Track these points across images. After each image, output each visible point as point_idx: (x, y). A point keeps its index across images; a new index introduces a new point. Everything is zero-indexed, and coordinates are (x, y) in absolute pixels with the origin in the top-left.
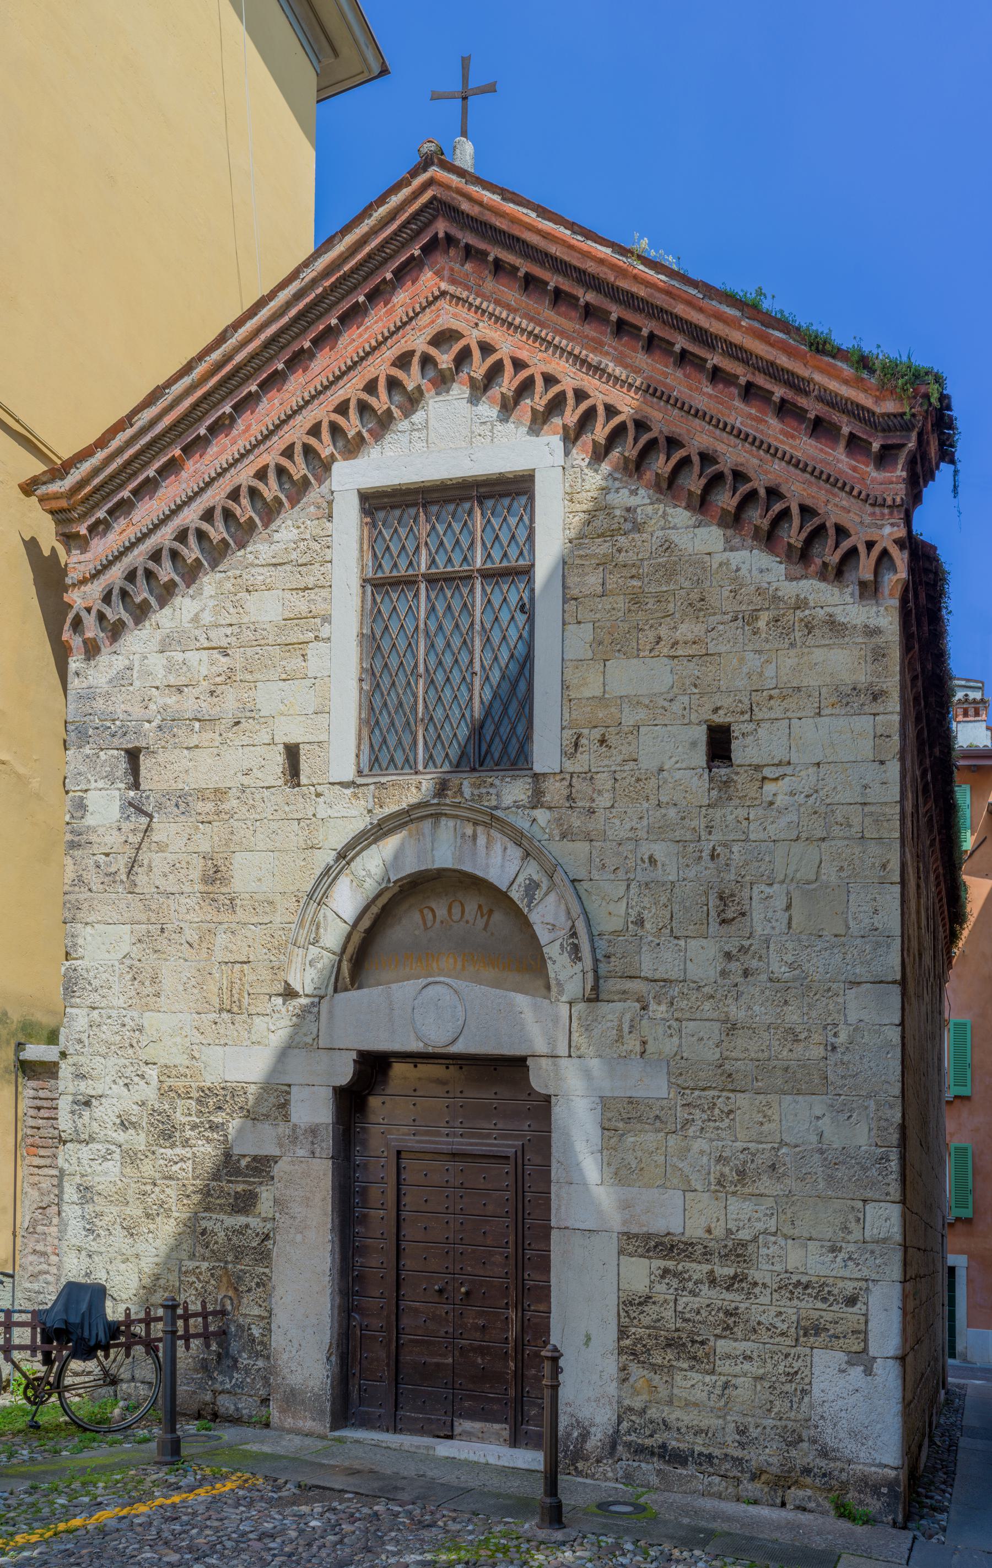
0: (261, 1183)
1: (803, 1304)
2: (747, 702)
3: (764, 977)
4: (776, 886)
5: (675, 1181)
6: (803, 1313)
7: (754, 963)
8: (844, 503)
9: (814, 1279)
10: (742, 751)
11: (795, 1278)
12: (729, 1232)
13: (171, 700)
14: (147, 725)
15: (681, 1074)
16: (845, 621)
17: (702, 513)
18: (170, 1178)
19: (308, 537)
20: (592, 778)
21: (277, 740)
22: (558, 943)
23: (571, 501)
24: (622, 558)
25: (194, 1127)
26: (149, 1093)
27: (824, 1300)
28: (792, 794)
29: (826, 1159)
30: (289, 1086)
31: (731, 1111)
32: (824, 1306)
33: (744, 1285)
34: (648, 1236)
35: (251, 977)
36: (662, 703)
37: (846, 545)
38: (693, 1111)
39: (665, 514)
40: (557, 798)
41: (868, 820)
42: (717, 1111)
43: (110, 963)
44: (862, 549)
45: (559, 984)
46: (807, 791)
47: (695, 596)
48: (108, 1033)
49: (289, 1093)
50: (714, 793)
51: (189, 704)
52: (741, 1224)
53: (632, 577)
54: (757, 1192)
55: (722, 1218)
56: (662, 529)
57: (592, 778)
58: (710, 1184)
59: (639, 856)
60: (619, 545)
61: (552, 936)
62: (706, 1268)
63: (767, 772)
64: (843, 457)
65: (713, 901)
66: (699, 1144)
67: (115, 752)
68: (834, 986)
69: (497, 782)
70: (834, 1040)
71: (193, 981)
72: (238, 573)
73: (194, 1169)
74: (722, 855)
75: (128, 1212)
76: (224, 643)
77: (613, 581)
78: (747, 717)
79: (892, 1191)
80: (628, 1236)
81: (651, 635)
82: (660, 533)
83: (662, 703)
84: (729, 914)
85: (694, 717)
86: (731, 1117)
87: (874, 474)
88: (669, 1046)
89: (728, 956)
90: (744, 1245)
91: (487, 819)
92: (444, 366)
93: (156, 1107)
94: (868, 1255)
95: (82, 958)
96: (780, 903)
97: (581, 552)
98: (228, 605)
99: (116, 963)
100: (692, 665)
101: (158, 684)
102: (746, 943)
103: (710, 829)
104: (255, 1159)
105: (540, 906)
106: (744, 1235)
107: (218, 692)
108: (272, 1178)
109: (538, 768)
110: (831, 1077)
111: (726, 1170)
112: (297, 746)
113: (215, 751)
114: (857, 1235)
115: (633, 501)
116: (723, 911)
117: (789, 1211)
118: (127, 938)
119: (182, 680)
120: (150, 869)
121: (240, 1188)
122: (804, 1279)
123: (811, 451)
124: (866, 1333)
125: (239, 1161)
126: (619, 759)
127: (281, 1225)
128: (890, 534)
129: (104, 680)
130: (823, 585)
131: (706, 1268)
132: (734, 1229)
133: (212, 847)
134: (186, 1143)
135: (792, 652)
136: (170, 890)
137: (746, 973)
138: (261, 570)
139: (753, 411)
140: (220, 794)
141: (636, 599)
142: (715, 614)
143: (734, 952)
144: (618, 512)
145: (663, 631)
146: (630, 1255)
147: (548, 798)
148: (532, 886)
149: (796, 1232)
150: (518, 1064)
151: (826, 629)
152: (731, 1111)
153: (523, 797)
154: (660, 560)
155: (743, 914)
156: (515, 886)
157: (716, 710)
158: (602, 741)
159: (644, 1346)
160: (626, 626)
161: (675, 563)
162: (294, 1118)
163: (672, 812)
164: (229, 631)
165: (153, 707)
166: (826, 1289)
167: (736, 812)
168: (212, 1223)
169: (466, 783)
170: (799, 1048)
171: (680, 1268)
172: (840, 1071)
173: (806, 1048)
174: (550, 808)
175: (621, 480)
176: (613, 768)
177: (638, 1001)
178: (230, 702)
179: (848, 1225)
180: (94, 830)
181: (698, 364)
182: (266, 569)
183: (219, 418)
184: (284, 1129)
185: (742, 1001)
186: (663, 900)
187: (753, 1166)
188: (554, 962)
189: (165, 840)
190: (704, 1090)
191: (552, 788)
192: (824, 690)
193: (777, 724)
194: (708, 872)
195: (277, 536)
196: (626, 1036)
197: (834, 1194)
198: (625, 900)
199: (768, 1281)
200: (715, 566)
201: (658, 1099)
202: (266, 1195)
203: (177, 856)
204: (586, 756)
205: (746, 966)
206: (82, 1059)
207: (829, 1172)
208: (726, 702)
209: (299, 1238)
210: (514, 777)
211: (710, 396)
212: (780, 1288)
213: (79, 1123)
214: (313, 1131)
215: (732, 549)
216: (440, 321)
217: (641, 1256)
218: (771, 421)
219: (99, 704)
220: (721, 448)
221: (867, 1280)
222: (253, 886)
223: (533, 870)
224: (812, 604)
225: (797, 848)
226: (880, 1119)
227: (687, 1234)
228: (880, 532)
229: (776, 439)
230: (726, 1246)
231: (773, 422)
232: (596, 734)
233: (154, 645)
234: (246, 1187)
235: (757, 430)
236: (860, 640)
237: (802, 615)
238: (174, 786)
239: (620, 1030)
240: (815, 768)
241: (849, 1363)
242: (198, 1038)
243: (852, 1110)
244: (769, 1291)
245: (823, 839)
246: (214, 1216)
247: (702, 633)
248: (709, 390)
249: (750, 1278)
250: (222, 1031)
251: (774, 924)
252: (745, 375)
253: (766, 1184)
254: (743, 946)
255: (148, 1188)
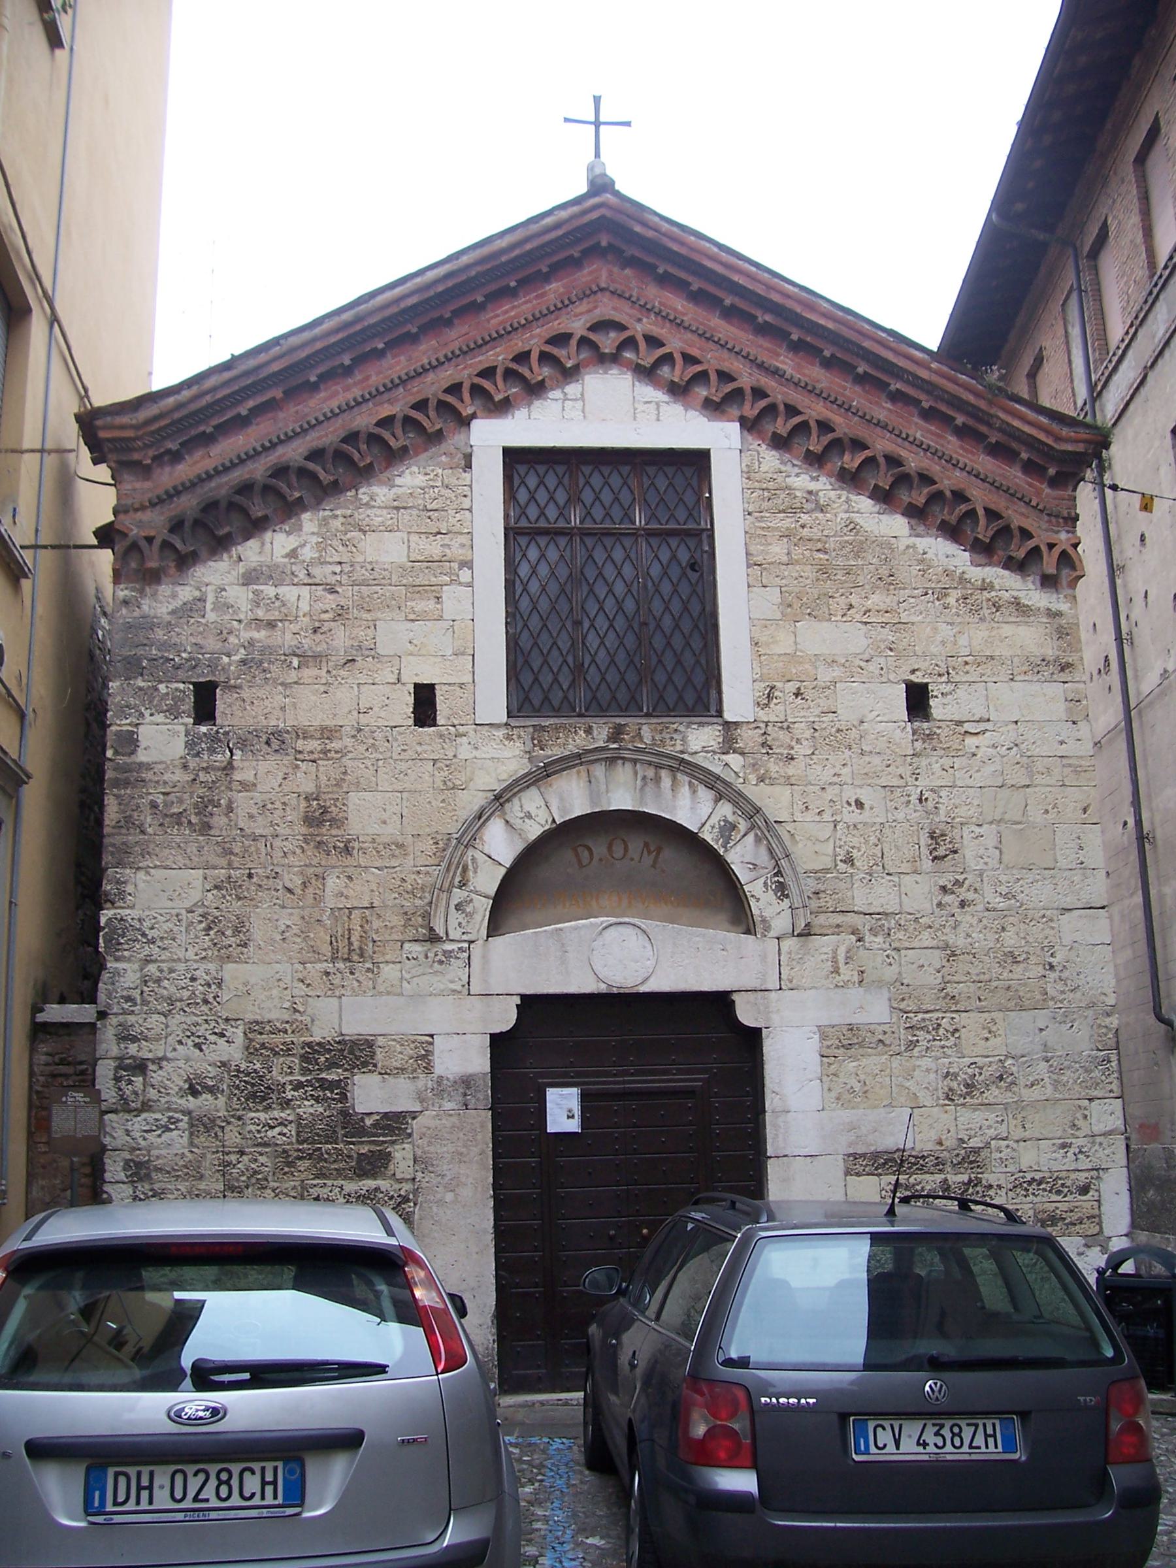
0: (393, 1142)
1: (1038, 1199)
2: (943, 666)
3: (980, 907)
4: (985, 826)
5: (902, 1099)
6: (1040, 1207)
7: (970, 896)
8: (1023, 510)
9: (1047, 1175)
10: (936, 706)
11: (1029, 1177)
12: (962, 1141)
13: (260, 635)
14: (225, 659)
15: (903, 999)
16: (1030, 603)
17: (885, 503)
18: (266, 1145)
19: (439, 484)
20: (788, 727)
21: (404, 679)
22: (762, 880)
23: (748, 478)
24: (805, 532)
25: (298, 1086)
26: (233, 1051)
27: (1059, 1192)
28: (994, 746)
29: (1051, 1066)
30: (432, 1036)
31: (956, 1030)
32: (1059, 1198)
33: (978, 1188)
34: (876, 1155)
35: (376, 924)
36: (858, 662)
37: (1031, 544)
38: (918, 1033)
39: (848, 501)
40: (751, 744)
41: (1067, 770)
42: (941, 1031)
43: (174, 912)
44: (1044, 548)
45: (764, 921)
46: (1008, 744)
47: (884, 572)
48: (173, 989)
49: (432, 1044)
50: (918, 745)
51: (285, 638)
52: (973, 1133)
53: (818, 550)
54: (987, 1101)
55: (953, 1129)
56: (847, 512)
57: (788, 727)
58: (938, 1098)
59: (845, 800)
60: (802, 521)
61: (753, 875)
62: (939, 1178)
63: (967, 727)
64: (1019, 474)
65: (924, 840)
66: (926, 1062)
67: (181, 686)
68: (1048, 913)
69: (681, 728)
70: (1051, 960)
71: (295, 930)
72: (349, 512)
73: (298, 1134)
74: (931, 799)
75: (202, 1187)
76: (332, 579)
77: (797, 553)
78: (944, 679)
79: (1115, 1089)
80: (855, 1156)
81: (843, 602)
82: (845, 516)
83: (858, 662)
84: (941, 852)
85: (892, 677)
86: (957, 1035)
87: (1048, 491)
88: (890, 973)
89: (944, 889)
90: (977, 1151)
91: (674, 764)
92: (607, 351)
93: (243, 1066)
94: (1097, 1147)
95: (132, 907)
96: (991, 841)
97: (763, 525)
98: (335, 543)
99: (183, 912)
100: (886, 630)
101: (242, 616)
102: (961, 878)
103: (916, 776)
104: (386, 1115)
105: (738, 847)
106: (975, 1143)
107: (324, 629)
108: (410, 1135)
109: (728, 716)
110: (1051, 992)
111: (954, 1085)
112: (431, 688)
113: (322, 688)
114: (1085, 1130)
115: (813, 486)
116: (935, 849)
117: (1019, 1116)
118: (198, 884)
119: (275, 615)
120: (230, 809)
121: (364, 1149)
122: (1038, 1176)
123: (989, 466)
124: (1100, 1216)
125: (362, 1120)
126: (817, 711)
127: (424, 1185)
128: (1068, 539)
129: (164, 610)
130: (1006, 573)
131: (939, 1178)
132: (966, 1139)
133: (318, 787)
134: (286, 1104)
135: (983, 626)
136: (258, 832)
137: (963, 904)
138: (379, 512)
139: (933, 428)
140: (328, 733)
141: (824, 571)
142: (904, 589)
143: (949, 886)
144: (798, 494)
145: (854, 600)
146: (858, 1174)
147: (741, 745)
148: (728, 829)
149: (1027, 1134)
150: (721, 1002)
151: (1012, 608)
152: (956, 1030)
153: (712, 743)
154: (846, 538)
155: (955, 852)
156: (707, 827)
157: (913, 672)
158: (797, 694)
159: (878, 1261)
160: (816, 592)
161: (862, 542)
162: (439, 1069)
163: (876, 760)
164: (338, 569)
165: (232, 639)
166: (1060, 1182)
167: (941, 761)
168: (326, 1190)
169: (645, 728)
170: (1019, 969)
171: (912, 1180)
172: (1060, 986)
173: (1026, 970)
174: (742, 754)
175: (800, 468)
176: (812, 719)
177: (853, 933)
178: (341, 639)
179: (1076, 1122)
180: (148, 767)
181: (882, 386)
182: (385, 511)
183: (334, 368)
184: (423, 1081)
185: (960, 930)
186: (873, 840)
187: (982, 1078)
188: (758, 900)
189: (252, 779)
190: (927, 1012)
191: (745, 735)
192: (1016, 660)
193: (974, 686)
194: (917, 814)
195: (398, 481)
196: (843, 968)
197: (1061, 1096)
198: (832, 841)
199: (1002, 1182)
200: (902, 548)
201: (879, 1024)
202: (402, 1156)
203: (270, 796)
204: (780, 707)
205: (962, 898)
206: (131, 1019)
207: (1055, 1077)
208: (923, 665)
209: (449, 1197)
210: (701, 724)
211: (890, 410)
212: (1015, 1187)
213: (128, 1091)
214: (466, 1082)
215: (918, 536)
216: (597, 311)
217: (868, 1174)
218: (950, 438)
219: (160, 634)
220: (904, 453)
221: (1097, 1170)
222: (375, 829)
223: (726, 810)
224: (997, 587)
225: (1005, 792)
226: (1100, 1026)
227: (918, 1148)
228: (1055, 536)
229: (956, 452)
230: (958, 1155)
231: (952, 439)
232: (791, 687)
233: (232, 577)
234: (373, 1148)
235: (937, 443)
236: (1045, 620)
237: (988, 596)
238: (265, 723)
239: (835, 960)
240: (1014, 726)
241: (1087, 1246)
242: (300, 989)
243: (1073, 1021)
244: (1004, 1191)
245: (1028, 786)
246: (329, 1183)
247: (894, 604)
248: (889, 405)
249: (984, 1182)
250: (336, 982)
251: (986, 860)
252: (927, 401)
253: (994, 1094)
254: (957, 880)
255: (233, 1158)
